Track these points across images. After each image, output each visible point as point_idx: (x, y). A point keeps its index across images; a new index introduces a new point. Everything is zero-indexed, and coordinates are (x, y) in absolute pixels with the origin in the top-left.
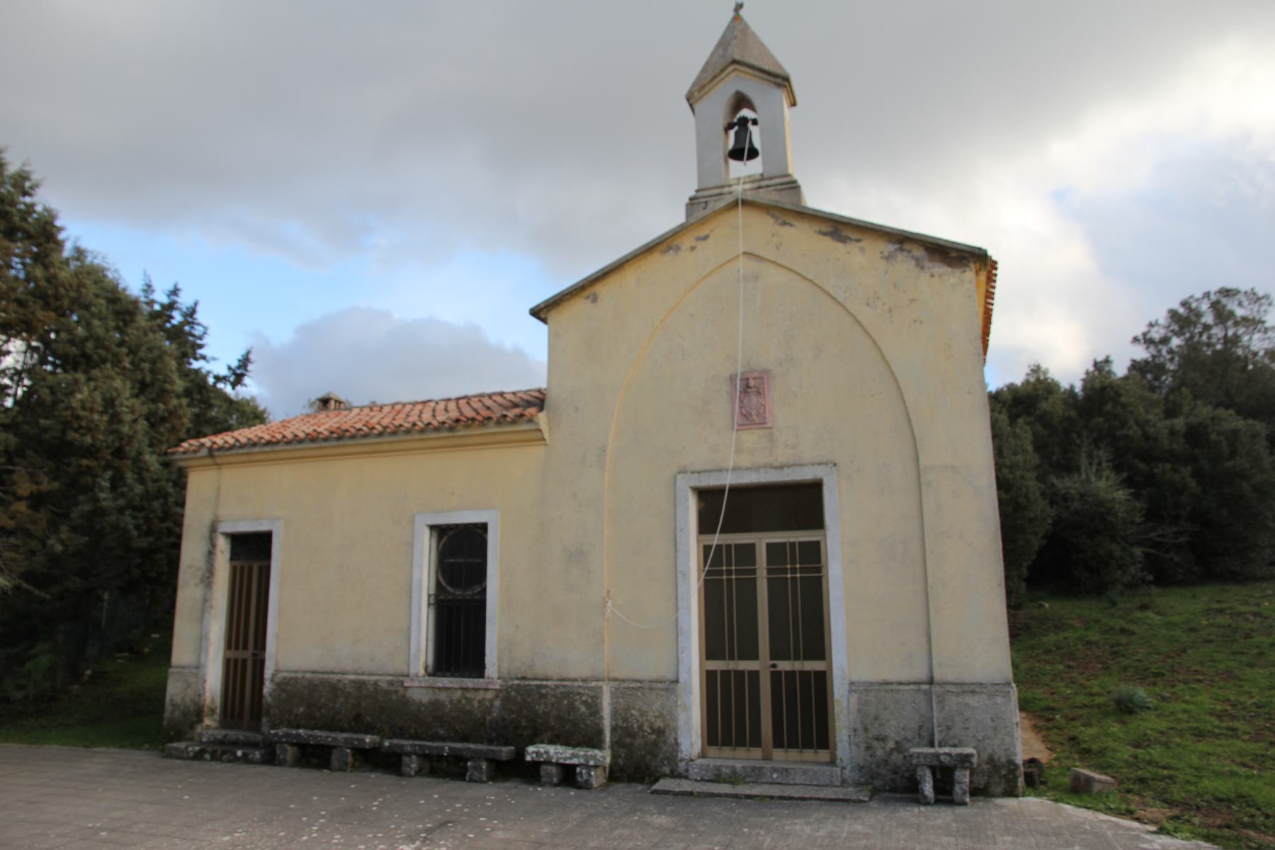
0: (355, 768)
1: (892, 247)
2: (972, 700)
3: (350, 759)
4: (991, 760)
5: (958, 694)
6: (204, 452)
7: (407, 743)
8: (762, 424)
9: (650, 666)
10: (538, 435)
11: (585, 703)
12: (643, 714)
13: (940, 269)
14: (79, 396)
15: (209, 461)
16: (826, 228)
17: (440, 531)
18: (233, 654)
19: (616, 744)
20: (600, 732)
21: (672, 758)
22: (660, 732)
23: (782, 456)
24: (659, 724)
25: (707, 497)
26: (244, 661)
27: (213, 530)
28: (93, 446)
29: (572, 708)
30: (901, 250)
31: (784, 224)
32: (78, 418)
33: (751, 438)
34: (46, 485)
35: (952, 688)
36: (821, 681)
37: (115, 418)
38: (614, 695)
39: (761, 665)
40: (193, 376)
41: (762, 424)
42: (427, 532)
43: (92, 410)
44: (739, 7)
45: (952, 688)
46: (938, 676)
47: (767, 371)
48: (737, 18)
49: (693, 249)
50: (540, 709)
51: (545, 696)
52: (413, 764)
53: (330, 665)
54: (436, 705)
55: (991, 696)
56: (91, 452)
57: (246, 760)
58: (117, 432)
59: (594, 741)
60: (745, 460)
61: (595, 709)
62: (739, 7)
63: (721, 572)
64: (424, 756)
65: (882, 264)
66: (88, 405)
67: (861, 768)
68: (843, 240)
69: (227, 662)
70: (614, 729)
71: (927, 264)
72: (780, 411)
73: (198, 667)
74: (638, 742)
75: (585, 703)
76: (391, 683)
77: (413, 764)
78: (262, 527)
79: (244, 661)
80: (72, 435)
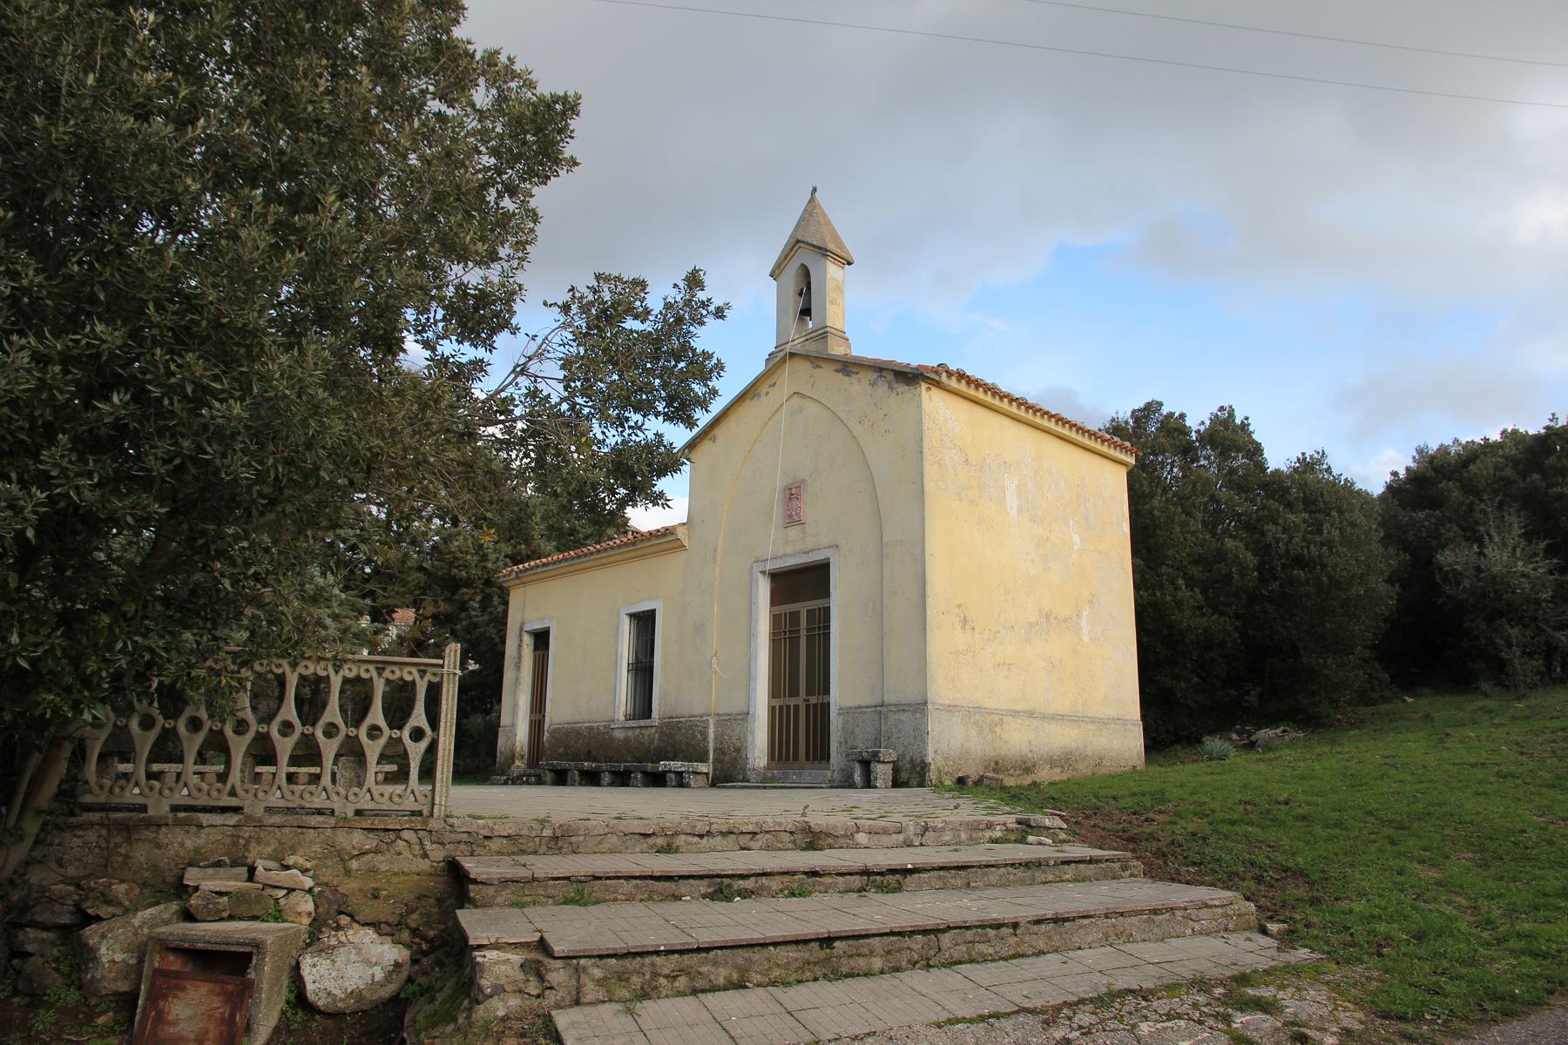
0: (581, 784)
1: (875, 375)
2: (903, 716)
3: (577, 778)
4: (911, 761)
5: (895, 712)
6: (514, 575)
7: (604, 766)
8: (799, 523)
9: (734, 705)
10: (678, 543)
11: (700, 732)
12: (730, 737)
13: (902, 388)
14: (456, 544)
15: (517, 581)
16: (839, 366)
17: (632, 616)
18: (777, 703)
19: (716, 760)
20: (707, 752)
21: (744, 769)
22: (738, 750)
23: (810, 543)
24: (738, 745)
25: (776, 577)
26: (796, 707)
27: (521, 629)
28: (468, 578)
29: (694, 736)
30: (881, 376)
31: (818, 366)
32: (458, 559)
33: (794, 532)
34: (443, 607)
35: (893, 708)
36: (826, 707)
37: (484, 558)
38: (717, 724)
39: (799, 701)
40: (1240, 461)
41: (799, 523)
42: (626, 620)
43: (467, 553)
44: (815, 190)
45: (893, 708)
46: (886, 702)
47: (804, 481)
48: (812, 200)
49: (767, 393)
50: (678, 738)
51: (680, 729)
52: (607, 778)
53: (578, 718)
54: (627, 739)
55: (914, 712)
56: (468, 583)
57: (528, 783)
58: (484, 567)
59: (703, 758)
60: (789, 549)
61: (705, 735)
62: (815, 190)
63: (814, 629)
64: (645, 773)
65: (869, 389)
66: (463, 549)
67: (843, 770)
68: (848, 374)
69: (772, 710)
70: (715, 750)
71: (895, 385)
72: (810, 510)
73: (513, 725)
74: (727, 758)
75: (700, 732)
76: (605, 727)
77: (607, 778)
78: (818, 557)
79: (796, 707)
80: (455, 571)
